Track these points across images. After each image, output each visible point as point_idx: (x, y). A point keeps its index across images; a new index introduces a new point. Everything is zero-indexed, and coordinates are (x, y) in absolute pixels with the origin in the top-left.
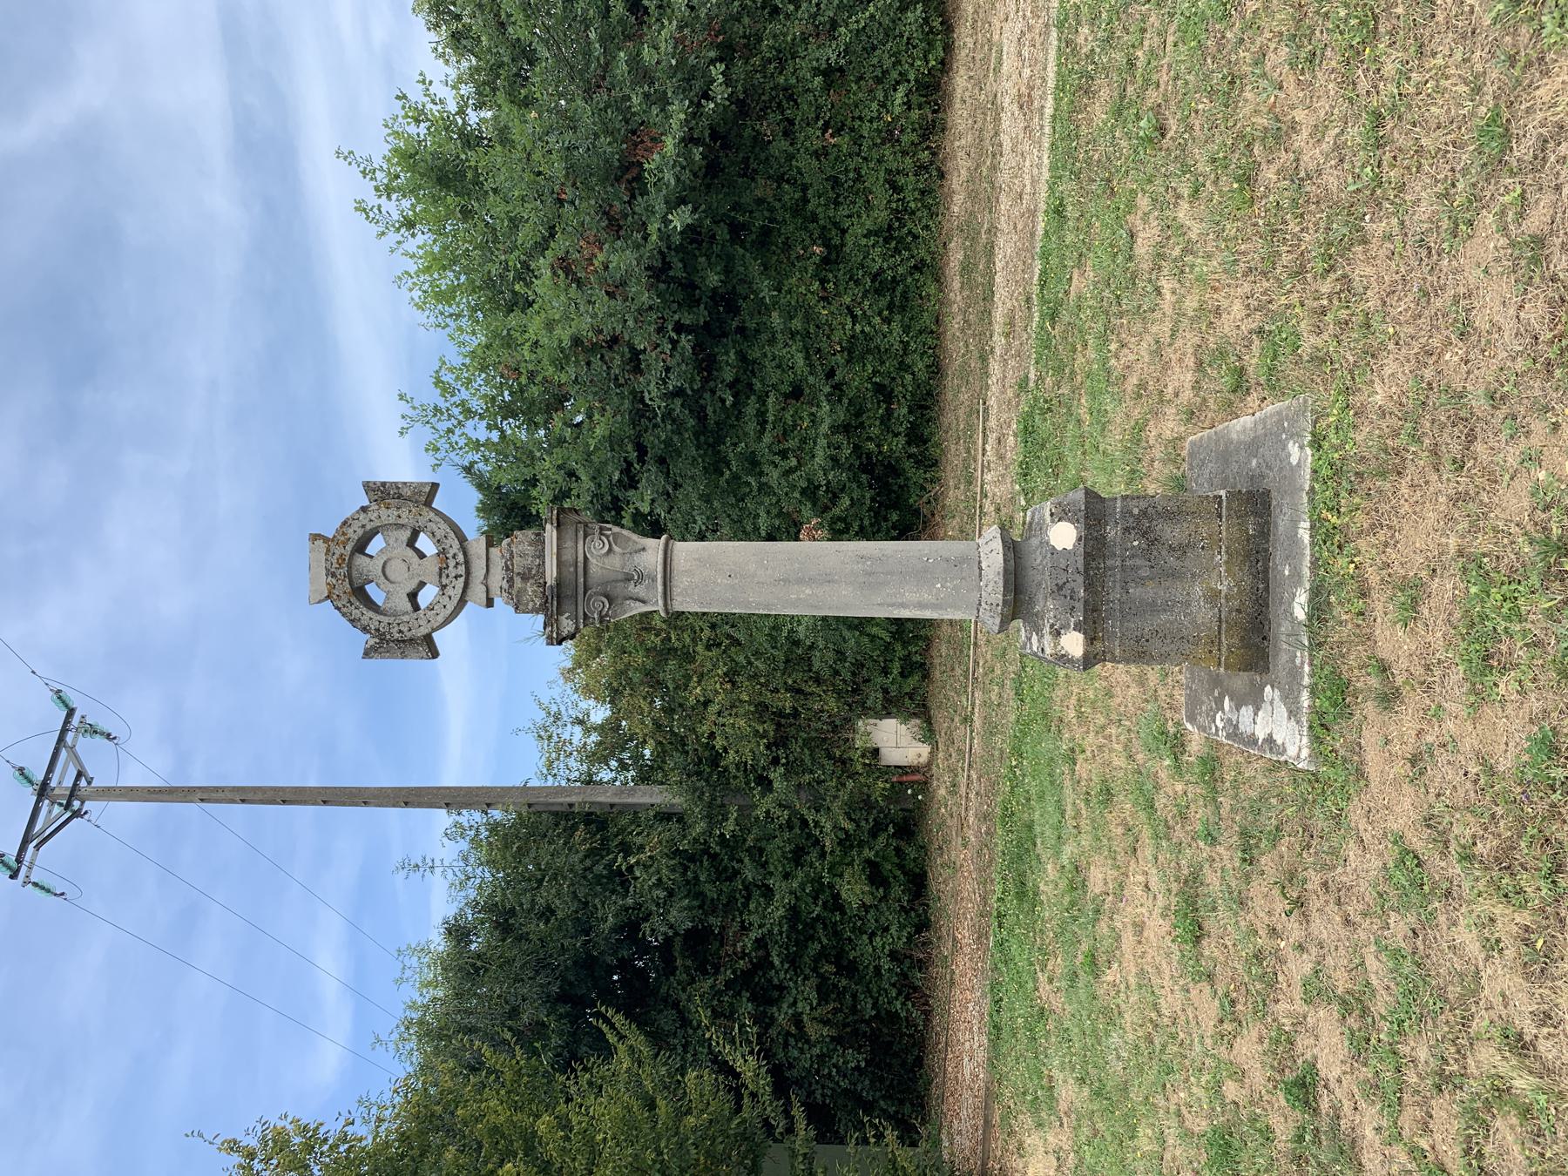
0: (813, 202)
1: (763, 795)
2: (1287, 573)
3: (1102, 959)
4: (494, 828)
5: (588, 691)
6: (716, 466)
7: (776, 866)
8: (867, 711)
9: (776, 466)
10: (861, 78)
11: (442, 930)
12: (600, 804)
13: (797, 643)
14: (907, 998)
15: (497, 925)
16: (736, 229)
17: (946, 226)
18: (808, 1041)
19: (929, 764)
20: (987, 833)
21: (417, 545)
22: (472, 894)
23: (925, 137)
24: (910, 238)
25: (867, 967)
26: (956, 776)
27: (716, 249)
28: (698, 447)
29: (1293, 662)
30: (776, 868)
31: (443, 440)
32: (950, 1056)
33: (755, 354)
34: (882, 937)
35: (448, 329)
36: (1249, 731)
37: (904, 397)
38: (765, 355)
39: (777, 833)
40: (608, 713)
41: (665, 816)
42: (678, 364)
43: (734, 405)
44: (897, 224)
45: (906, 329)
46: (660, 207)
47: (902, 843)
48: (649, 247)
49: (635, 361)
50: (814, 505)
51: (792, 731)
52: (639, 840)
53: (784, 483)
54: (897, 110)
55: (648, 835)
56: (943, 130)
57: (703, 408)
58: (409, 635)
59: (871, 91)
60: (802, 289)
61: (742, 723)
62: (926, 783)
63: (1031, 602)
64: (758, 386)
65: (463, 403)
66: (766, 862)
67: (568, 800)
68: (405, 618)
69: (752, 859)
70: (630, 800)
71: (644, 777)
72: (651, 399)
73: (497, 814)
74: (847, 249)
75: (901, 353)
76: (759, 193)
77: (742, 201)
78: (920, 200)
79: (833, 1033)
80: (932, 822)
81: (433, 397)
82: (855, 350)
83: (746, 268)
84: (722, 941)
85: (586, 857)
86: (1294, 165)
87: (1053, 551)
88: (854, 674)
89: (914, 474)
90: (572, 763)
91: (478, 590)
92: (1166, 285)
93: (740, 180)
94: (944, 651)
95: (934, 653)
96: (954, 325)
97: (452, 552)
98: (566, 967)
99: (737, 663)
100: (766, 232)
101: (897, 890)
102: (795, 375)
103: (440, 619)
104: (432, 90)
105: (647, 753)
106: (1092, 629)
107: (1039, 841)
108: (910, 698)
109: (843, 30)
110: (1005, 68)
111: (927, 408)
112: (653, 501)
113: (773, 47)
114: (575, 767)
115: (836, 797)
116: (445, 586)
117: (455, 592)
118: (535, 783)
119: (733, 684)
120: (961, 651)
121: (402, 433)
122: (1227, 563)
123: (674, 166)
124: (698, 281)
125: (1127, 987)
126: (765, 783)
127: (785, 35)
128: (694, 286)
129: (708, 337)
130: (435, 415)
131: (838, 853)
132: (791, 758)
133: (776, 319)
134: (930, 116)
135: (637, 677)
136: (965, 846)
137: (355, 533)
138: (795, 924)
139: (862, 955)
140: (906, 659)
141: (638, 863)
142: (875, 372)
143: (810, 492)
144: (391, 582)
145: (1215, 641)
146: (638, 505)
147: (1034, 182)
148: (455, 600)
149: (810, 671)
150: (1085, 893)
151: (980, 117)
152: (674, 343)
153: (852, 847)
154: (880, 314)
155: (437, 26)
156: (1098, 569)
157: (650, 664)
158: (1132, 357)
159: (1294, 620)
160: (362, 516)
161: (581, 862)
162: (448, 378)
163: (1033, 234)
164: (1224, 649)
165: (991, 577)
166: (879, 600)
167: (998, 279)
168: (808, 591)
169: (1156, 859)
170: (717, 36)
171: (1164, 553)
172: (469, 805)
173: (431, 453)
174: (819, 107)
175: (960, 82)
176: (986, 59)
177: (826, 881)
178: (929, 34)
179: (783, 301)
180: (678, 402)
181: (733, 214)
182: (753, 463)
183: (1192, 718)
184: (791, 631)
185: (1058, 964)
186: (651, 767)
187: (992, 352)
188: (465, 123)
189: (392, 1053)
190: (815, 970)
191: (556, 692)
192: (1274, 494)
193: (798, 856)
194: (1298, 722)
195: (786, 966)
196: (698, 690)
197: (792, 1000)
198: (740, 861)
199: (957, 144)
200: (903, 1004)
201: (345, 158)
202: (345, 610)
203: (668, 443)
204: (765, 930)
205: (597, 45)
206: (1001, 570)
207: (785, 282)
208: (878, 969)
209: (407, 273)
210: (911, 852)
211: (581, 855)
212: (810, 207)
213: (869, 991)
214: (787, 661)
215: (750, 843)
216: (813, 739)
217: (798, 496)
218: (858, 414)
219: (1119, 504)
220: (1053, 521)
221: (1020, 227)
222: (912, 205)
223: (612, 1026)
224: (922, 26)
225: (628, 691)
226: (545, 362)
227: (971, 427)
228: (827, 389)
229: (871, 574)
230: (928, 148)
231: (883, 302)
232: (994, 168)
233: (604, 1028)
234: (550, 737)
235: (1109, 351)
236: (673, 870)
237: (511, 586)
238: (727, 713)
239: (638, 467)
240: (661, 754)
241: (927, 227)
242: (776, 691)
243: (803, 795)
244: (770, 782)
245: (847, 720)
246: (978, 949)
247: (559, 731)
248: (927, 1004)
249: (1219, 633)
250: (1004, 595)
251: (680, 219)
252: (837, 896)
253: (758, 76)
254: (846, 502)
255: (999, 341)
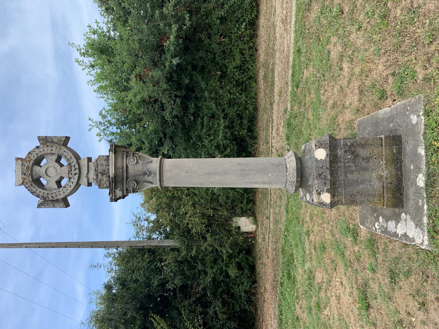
0: (217, 58)
1: (204, 242)
2: (412, 168)
3: (322, 306)
4: (120, 254)
5: (149, 211)
6: (188, 139)
7: (208, 264)
8: (236, 215)
9: (207, 139)
10: (231, 21)
11: (103, 287)
12: (153, 246)
13: (214, 194)
14: (250, 305)
15: (121, 284)
16: (194, 68)
17: (258, 65)
18: (219, 319)
19: (256, 231)
20: (276, 255)
21: (61, 162)
22: (113, 274)
23: (251, 39)
24: (247, 69)
25: (237, 295)
26: (265, 235)
27: (188, 72)
28: (183, 134)
29: (418, 204)
30: (208, 265)
31: (102, 132)
32: (264, 324)
33: (200, 105)
34: (242, 286)
35: (104, 99)
36: (394, 230)
37: (246, 118)
38: (203, 105)
39: (209, 254)
40: (156, 217)
41: (173, 249)
42: (176, 108)
43: (194, 120)
44: (243, 65)
45: (247, 97)
46: (169, 57)
47: (248, 256)
48: (166, 70)
49: (162, 108)
50: (219, 151)
51: (213, 221)
52: (165, 258)
53: (210, 144)
54: (243, 30)
55: (168, 255)
56: (257, 37)
57: (184, 122)
58: (56, 198)
59: (234, 25)
60: (214, 85)
61: (197, 220)
62: (255, 237)
63: (307, 181)
64: (201, 114)
65: (109, 121)
66: (205, 263)
67: (143, 245)
68: (54, 191)
69: (201, 263)
70: (162, 244)
71: (167, 237)
72: (167, 118)
73: (120, 249)
74: (228, 73)
75: (245, 104)
76: (200, 55)
77: (196, 58)
78: (250, 58)
79: (227, 317)
80: (257, 250)
81: (100, 119)
82: (231, 103)
83: (197, 78)
84: (192, 288)
85: (148, 263)
86: (411, 4)
87: (317, 160)
88: (232, 203)
89: (249, 141)
90: (144, 233)
91: (84, 180)
92: (345, 66)
93: (195, 51)
94: (260, 196)
95: (257, 196)
96: (261, 95)
97: (73, 164)
98: (142, 298)
99: (195, 201)
100: (203, 68)
101: (246, 271)
102: (212, 111)
103: (69, 191)
104: (99, 25)
105: (168, 229)
106: (333, 192)
107: (295, 260)
108: (250, 211)
109: (226, 6)
110: (277, 13)
111: (253, 121)
112: (168, 150)
113: (204, 11)
114: (145, 234)
115: (227, 242)
116: (71, 178)
117: (75, 181)
118: (132, 239)
119: (194, 207)
120: (266, 196)
121: (89, 130)
122: (385, 164)
123: (173, 45)
124: (182, 82)
125: (334, 319)
126: (205, 238)
127: (208, 7)
128: (181, 84)
129: (185, 100)
130: (100, 125)
131: (227, 260)
132: (213, 230)
133: (206, 94)
134: (253, 32)
135: (164, 206)
136: (268, 258)
137: (34, 157)
138: (215, 282)
139: (236, 291)
140: (248, 198)
141: (164, 265)
142: (237, 110)
143: (218, 147)
144: (49, 177)
145: (382, 196)
146: (163, 151)
147: (288, 46)
148: (75, 183)
149: (219, 202)
150: (314, 281)
151: (269, 29)
152: (175, 101)
153: (232, 258)
154: (238, 92)
155: (101, 6)
156: (335, 167)
157: (168, 202)
158: (330, 94)
159: (417, 187)
160: (37, 150)
161: (147, 264)
162: (104, 113)
163: (288, 63)
164: (386, 199)
165: (291, 171)
166: (247, 181)
167: (276, 79)
168: (218, 178)
169: (346, 274)
170: (187, 8)
171: (361, 160)
172: (112, 247)
173: (98, 136)
174: (219, 30)
175: (262, 21)
176: (270, 13)
177: (224, 269)
178: (252, 7)
179: (208, 88)
180: (176, 119)
181: (192, 61)
182: (200, 138)
183: (363, 224)
184: (212, 190)
185: (304, 303)
186: (169, 233)
187: (274, 102)
188: (110, 35)
189: (87, 327)
190: (221, 296)
191: (139, 211)
192: (403, 136)
193: (215, 261)
194: (421, 229)
195: (212, 296)
196: (183, 209)
197: (214, 306)
198: (197, 263)
199: (261, 40)
200: (249, 306)
201: (71, 45)
202: (29, 188)
203: (173, 132)
204: (205, 285)
205: (149, 9)
206: (295, 168)
207: (209, 83)
208: (240, 296)
209: (91, 80)
210: (250, 259)
211: (146, 263)
212: (216, 60)
213: (238, 302)
214: (211, 200)
215: (200, 257)
216: (220, 224)
217: (214, 148)
218: (232, 123)
219: (342, 141)
220: (316, 148)
221: (283, 61)
222: (248, 59)
223: (155, 320)
224: (250, 5)
225: (161, 210)
226: (134, 107)
227: (267, 126)
228: (223, 115)
229: (243, 170)
230: (252, 42)
231: (239, 89)
232: (274, 45)
233: (153, 321)
234: (137, 225)
235: (320, 94)
236: (175, 267)
237: (97, 178)
238: (192, 216)
239: (163, 140)
240: (172, 230)
241: (252, 66)
242: (208, 209)
243: (217, 242)
244: (206, 238)
245: (230, 218)
246: (273, 292)
247: (140, 223)
248: (256, 306)
249: (383, 192)
250: (297, 178)
251: (175, 61)
252: (227, 273)
253: (200, 20)
254: (229, 150)
255: (276, 98)
